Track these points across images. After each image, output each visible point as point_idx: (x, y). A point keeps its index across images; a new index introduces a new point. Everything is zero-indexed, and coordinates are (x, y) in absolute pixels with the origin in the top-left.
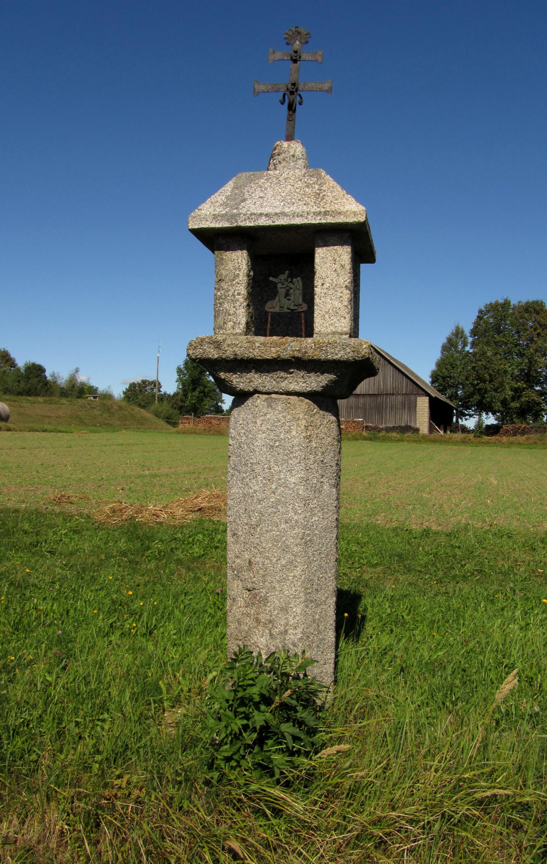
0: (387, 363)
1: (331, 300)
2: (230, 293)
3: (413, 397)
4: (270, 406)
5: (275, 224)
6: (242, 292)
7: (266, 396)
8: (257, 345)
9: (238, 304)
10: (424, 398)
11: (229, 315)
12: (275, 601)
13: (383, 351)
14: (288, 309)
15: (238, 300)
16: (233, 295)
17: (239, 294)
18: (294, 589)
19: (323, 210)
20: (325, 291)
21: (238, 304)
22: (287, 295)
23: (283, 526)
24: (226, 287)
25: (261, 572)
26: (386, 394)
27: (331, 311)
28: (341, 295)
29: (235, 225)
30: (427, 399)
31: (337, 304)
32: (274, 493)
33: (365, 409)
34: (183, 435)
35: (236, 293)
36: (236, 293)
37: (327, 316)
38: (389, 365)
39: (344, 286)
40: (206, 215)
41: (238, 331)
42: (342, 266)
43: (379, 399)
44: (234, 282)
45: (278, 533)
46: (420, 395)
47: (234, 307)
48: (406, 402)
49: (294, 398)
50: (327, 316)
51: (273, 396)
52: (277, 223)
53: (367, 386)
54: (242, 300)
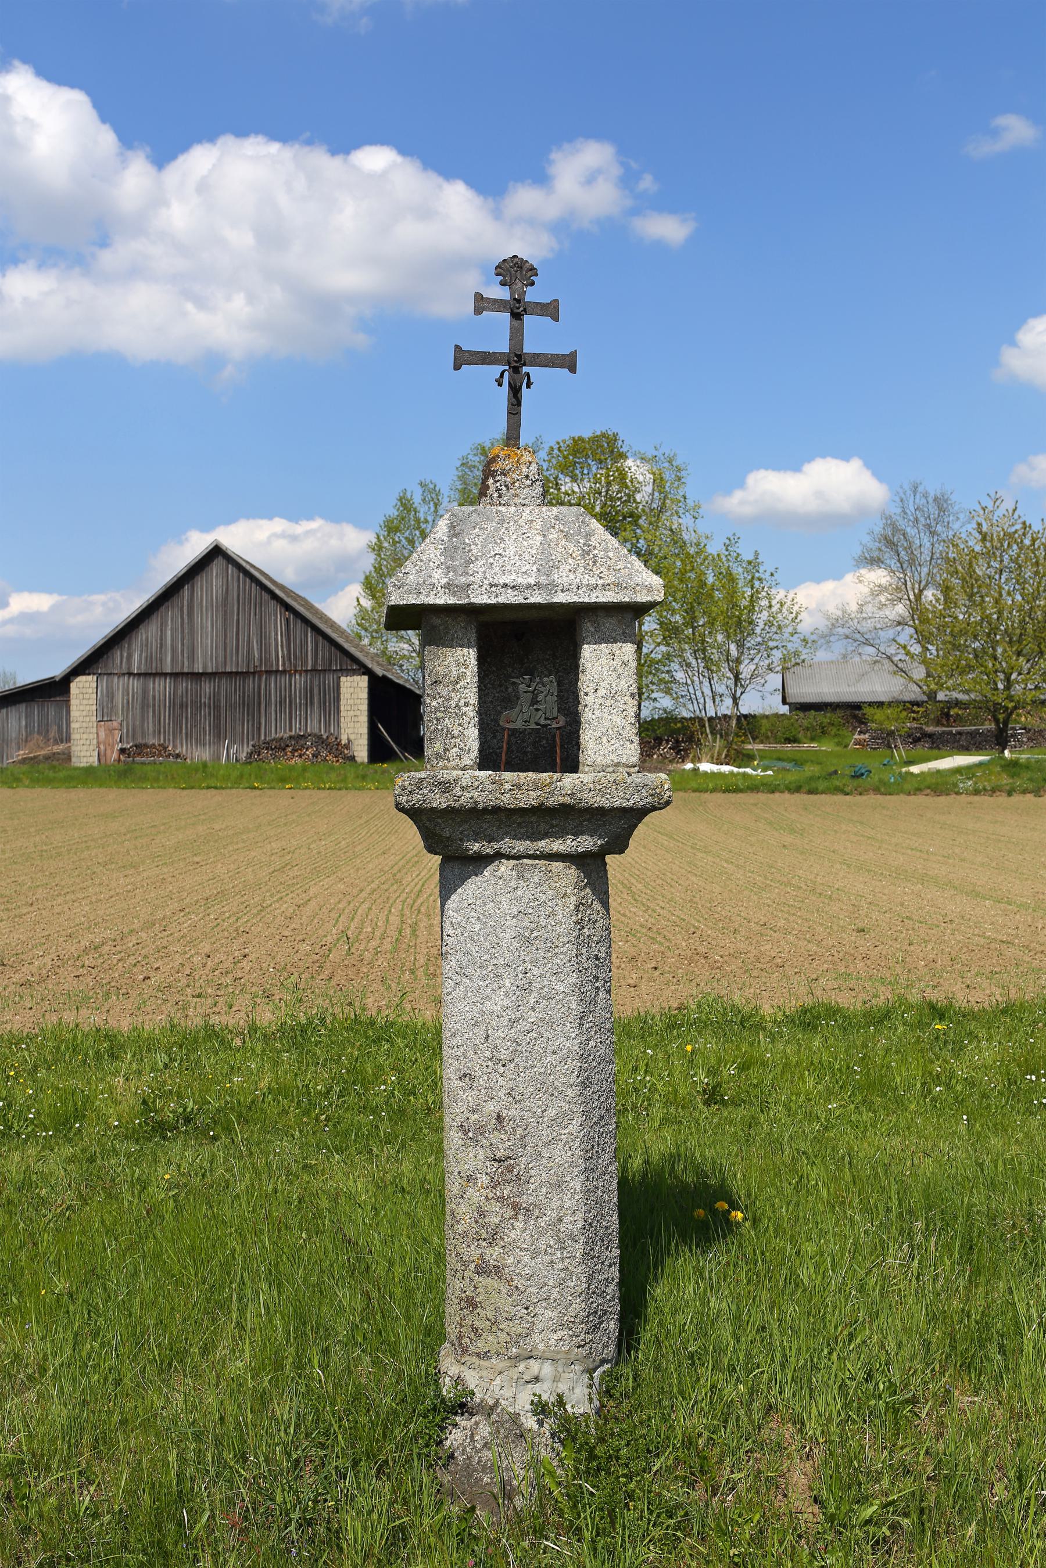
0: (266, 596)
1: (610, 714)
2: (453, 703)
3: (330, 678)
5: (528, 601)
6: (472, 702)
7: (515, 862)
8: (507, 786)
10: (357, 678)
11: (453, 737)
12: (540, 1175)
13: (248, 562)
14: (537, 724)
15: (465, 714)
16: (457, 705)
17: (466, 705)
19: (601, 582)
22: (534, 702)
23: (549, 1059)
24: (445, 693)
25: (520, 1131)
26: (269, 672)
27: (610, 731)
28: (624, 707)
29: (466, 601)
30: (363, 681)
31: (619, 720)
32: (533, 1009)
33: (217, 708)
35: (462, 703)
36: (462, 703)
37: (604, 739)
38: (273, 603)
40: (418, 584)
41: (469, 762)
42: (625, 664)
43: (250, 683)
44: (458, 686)
46: (353, 672)
47: (459, 725)
48: (316, 691)
49: (557, 866)
50: (604, 739)
51: (525, 861)
52: (532, 600)
53: (221, 653)
54: (472, 714)
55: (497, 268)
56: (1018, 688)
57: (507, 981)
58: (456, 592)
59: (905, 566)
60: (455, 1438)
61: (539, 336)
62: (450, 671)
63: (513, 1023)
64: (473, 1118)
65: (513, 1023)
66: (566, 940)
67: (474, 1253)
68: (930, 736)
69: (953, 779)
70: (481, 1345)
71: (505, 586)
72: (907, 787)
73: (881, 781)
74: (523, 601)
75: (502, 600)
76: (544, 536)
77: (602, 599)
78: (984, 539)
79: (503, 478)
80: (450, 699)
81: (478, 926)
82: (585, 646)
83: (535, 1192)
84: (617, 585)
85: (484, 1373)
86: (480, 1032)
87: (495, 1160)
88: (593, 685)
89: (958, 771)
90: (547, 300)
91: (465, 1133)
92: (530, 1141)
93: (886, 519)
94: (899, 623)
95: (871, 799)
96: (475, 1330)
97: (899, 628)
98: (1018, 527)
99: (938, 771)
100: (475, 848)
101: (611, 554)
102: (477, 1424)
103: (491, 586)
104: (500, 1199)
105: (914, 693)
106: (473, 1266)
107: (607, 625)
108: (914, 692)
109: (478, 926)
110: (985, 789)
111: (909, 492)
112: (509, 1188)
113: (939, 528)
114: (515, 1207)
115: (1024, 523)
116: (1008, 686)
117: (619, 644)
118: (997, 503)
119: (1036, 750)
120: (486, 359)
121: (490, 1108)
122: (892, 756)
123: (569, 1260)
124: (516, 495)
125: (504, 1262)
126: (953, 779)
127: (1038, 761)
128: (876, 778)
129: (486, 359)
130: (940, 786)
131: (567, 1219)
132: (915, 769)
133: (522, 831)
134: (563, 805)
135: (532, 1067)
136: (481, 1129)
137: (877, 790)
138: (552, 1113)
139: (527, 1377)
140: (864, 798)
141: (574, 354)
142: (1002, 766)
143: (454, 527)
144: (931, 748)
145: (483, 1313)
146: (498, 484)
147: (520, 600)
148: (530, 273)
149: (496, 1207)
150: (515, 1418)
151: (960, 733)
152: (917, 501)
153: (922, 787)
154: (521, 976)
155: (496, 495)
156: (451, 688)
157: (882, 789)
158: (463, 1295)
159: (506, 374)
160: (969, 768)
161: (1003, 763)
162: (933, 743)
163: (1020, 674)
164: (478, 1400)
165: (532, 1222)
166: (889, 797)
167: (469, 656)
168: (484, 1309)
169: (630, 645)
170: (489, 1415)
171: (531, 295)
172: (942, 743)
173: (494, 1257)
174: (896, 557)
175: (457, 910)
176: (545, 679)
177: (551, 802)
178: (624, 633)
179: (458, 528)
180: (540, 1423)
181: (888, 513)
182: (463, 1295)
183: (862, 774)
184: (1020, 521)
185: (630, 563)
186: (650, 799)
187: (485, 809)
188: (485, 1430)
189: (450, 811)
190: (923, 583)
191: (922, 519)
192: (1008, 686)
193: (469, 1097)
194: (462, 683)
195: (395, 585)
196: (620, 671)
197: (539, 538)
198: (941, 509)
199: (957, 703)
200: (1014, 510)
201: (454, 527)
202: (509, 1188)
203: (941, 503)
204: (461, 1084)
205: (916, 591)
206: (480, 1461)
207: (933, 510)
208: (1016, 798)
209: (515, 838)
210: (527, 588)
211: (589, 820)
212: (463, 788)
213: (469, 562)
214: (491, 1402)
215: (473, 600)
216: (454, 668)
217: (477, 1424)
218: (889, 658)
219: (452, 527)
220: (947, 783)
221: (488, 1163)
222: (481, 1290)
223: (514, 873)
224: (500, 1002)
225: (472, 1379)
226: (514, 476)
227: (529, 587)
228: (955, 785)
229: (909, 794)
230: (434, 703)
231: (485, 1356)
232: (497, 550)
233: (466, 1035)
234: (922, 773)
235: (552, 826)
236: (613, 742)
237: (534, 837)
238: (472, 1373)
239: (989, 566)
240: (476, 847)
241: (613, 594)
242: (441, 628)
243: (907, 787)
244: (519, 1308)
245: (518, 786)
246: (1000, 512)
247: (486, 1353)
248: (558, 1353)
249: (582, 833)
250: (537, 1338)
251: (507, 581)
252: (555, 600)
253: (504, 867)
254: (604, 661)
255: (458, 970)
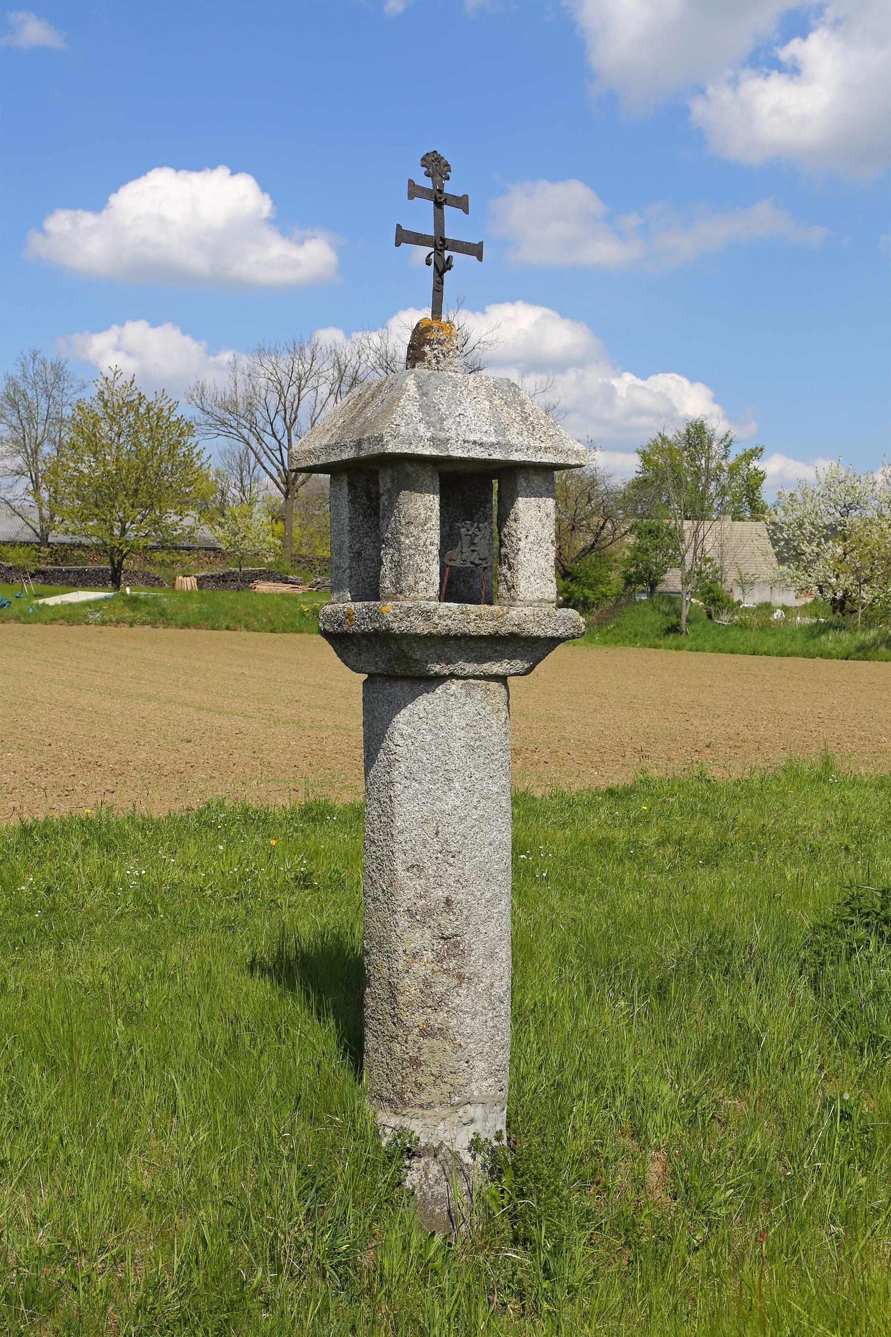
2: (421, 542)
4: (468, 694)
5: (491, 457)
6: (436, 542)
9: (432, 557)
12: (479, 949)
14: (472, 563)
15: (430, 552)
16: (425, 544)
17: (432, 544)
18: (500, 928)
20: (530, 546)
21: (432, 557)
24: (415, 533)
25: (465, 912)
31: (543, 563)
34: (66, 629)
35: (428, 543)
36: (428, 543)
39: (550, 541)
41: (434, 595)
45: (482, 859)
47: (427, 561)
50: (532, 579)
51: (471, 681)
52: (494, 457)
55: (423, 159)
56: (131, 534)
57: (457, 785)
58: (438, 445)
59: (24, 422)
60: (412, 1179)
61: (456, 226)
62: (420, 514)
63: (462, 819)
64: (421, 903)
65: (462, 819)
66: (499, 748)
67: (419, 1018)
68: (43, 573)
69: (84, 611)
70: (424, 1097)
71: (475, 442)
72: (44, 617)
73: (21, 611)
74: (487, 457)
75: (472, 454)
76: (491, 401)
77: (544, 460)
78: (106, 406)
79: (440, 347)
80: (419, 538)
81: (429, 737)
82: (520, 499)
83: (475, 963)
84: (556, 449)
85: (428, 1121)
86: (430, 829)
87: (442, 938)
88: (524, 532)
89: (87, 604)
90: (459, 195)
91: (412, 916)
92: (473, 920)
93: (9, 379)
94: (18, 473)
95: (13, 627)
96: (418, 1085)
97: (17, 477)
98: (135, 397)
99: (70, 604)
100: (436, 670)
101: (542, 421)
102: (427, 1164)
103: (465, 442)
104: (446, 971)
105: (27, 535)
106: (416, 1030)
107: (536, 481)
108: (29, 534)
109: (429, 737)
110: (111, 621)
111: (29, 358)
112: (454, 962)
113: (55, 393)
114: (460, 977)
115: (140, 394)
116: (124, 531)
117: (544, 499)
118: (117, 375)
119: (156, 589)
120: (418, 239)
121: (440, 893)
122: (22, 590)
123: (497, 1019)
124: (451, 363)
125: (448, 1025)
126: (84, 611)
127: (154, 598)
128: (17, 608)
129: (418, 239)
130: (71, 616)
131: (497, 984)
132: (51, 601)
133: (473, 655)
134: (512, 634)
135: (475, 857)
136: (429, 912)
137: (17, 619)
138: (488, 895)
139: (465, 1120)
140: (7, 626)
141: (481, 244)
142: (124, 601)
143: (421, 387)
144: (44, 583)
145: (427, 1070)
146: (436, 352)
147: (485, 456)
148: (446, 169)
149: (444, 978)
150: (456, 1156)
151: (69, 572)
152: (36, 366)
153: (57, 617)
154: (468, 779)
155: (434, 361)
156: (420, 529)
157: (21, 618)
158: (406, 1056)
159: (432, 257)
160: (96, 602)
161: (125, 598)
162: (45, 579)
163: (132, 523)
164: (423, 1145)
165: (473, 989)
166: (28, 626)
167: (437, 499)
168: (427, 1066)
169: (552, 500)
170: (435, 1156)
171: (450, 188)
172: (54, 579)
173: (439, 1021)
174: (16, 414)
175: (408, 723)
176: (481, 525)
177: (503, 631)
178: (547, 489)
179: (424, 388)
180: (474, 1157)
181: (10, 375)
182: (406, 1056)
183: (4, 605)
184: (137, 392)
185: (558, 430)
186: (572, 630)
187: (455, 635)
188: (435, 1169)
189: (430, 637)
190: (40, 439)
191: (40, 384)
192: (124, 531)
193: (419, 884)
194: (428, 525)
195: (391, 435)
196: (544, 521)
197: (487, 403)
198: (58, 377)
199: (80, 546)
200: (132, 383)
201: (421, 387)
202: (454, 962)
203: (58, 372)
204: (408, 874)
205: (33, 446)
206: (433, 1195)
207: (51, 377)
208: (137, 629)
209: (467, 661)
210: (491, 446)
211: (522, 647)
212: (440, 617)
213: (442, 420)
214: (436, 1145)
215: (452, 453)
216: (422, 511)
217: (427, 1164)
218: (7, 503)
219: (419, 387)
220: (78, 615)
221: (434, 941)
222: (425, 1050)
223: (463, 691)
224: (451, 802)
225: (415, 1126)
226: (448, 346)
227: (492, 445)
228: (86, 616)
229: (46, 623)
230: (407, 541)
231: (430, 1106)
232: (460, 410)
233: (415, 832)
234: (57, 605)
235: (496, 651)
236: (538, 581)
237: (480, 660)
238: (415, 1122)
239: (111, 429)
240: (437, 668)
241: (552, 456)
242: (414, 475)
243: (44, 617)
244: (462, 1062)
245: (480, 616)
246: (119, 383)
247: (429, 1103)
248: (487, 1097)
249: (515, 658)
250: (473, 1086)
251: (476, 439)
252: (511, 458)
253: (454, 686)
254: (533, 512)
255: (408, 775)
